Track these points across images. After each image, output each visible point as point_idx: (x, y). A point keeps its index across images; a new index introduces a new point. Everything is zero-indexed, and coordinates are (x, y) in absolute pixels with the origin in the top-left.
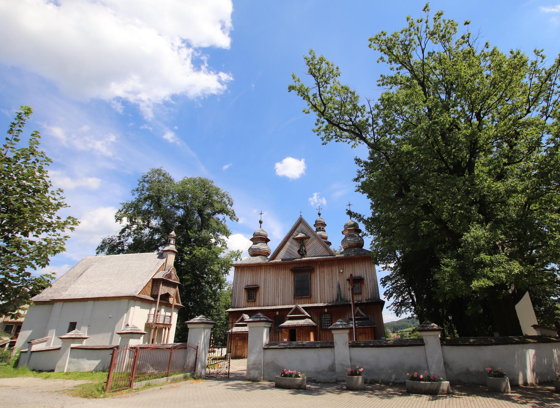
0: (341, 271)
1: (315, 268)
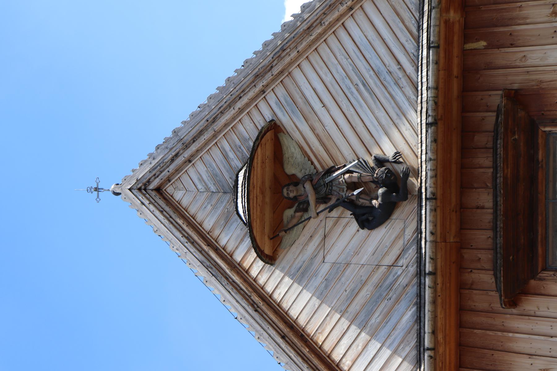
1: (516, 80)
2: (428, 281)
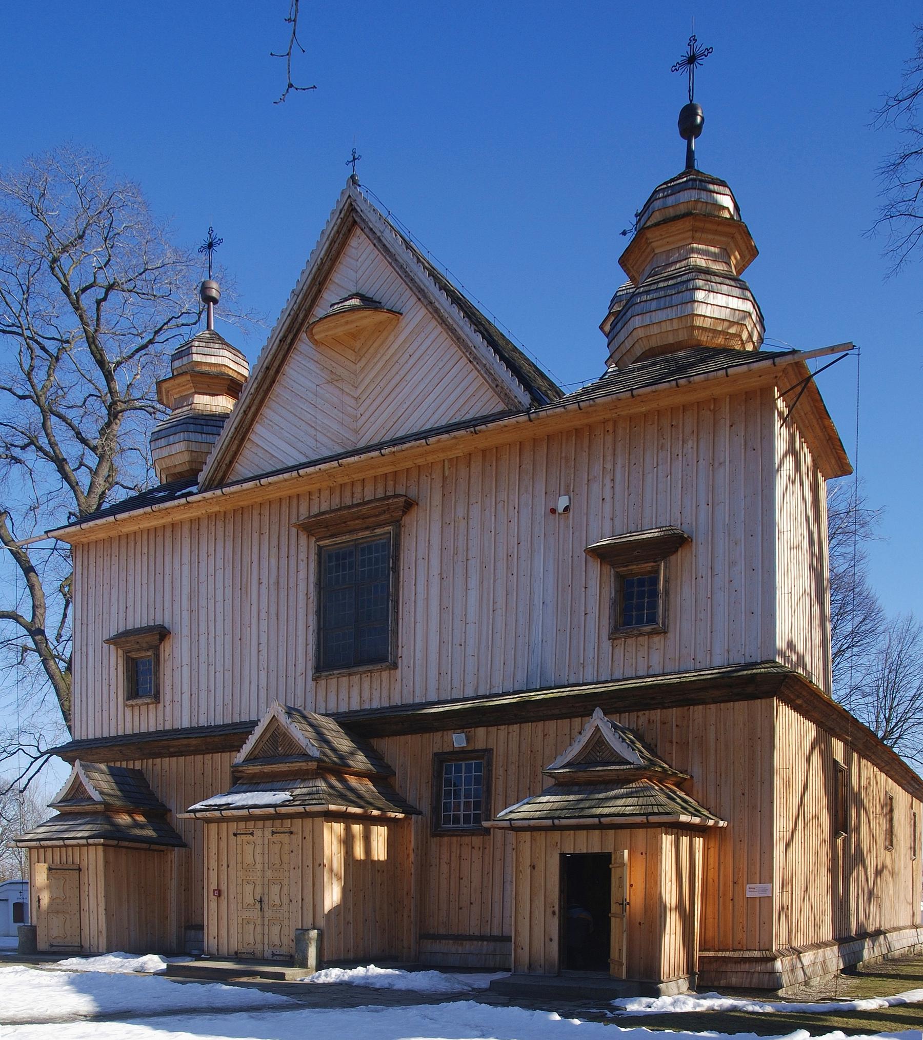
0: (563, 502)
2: (295, 473)
